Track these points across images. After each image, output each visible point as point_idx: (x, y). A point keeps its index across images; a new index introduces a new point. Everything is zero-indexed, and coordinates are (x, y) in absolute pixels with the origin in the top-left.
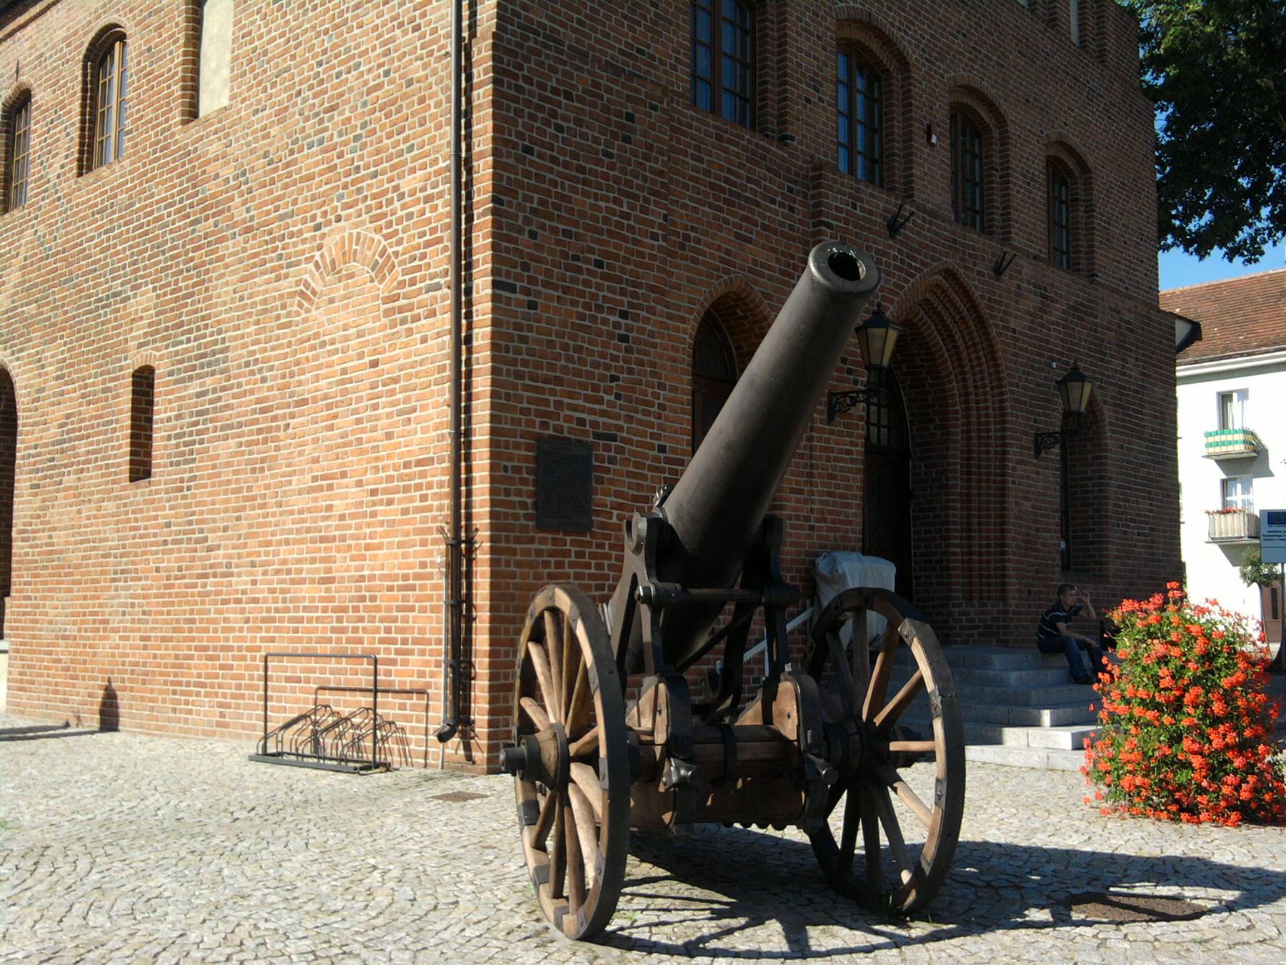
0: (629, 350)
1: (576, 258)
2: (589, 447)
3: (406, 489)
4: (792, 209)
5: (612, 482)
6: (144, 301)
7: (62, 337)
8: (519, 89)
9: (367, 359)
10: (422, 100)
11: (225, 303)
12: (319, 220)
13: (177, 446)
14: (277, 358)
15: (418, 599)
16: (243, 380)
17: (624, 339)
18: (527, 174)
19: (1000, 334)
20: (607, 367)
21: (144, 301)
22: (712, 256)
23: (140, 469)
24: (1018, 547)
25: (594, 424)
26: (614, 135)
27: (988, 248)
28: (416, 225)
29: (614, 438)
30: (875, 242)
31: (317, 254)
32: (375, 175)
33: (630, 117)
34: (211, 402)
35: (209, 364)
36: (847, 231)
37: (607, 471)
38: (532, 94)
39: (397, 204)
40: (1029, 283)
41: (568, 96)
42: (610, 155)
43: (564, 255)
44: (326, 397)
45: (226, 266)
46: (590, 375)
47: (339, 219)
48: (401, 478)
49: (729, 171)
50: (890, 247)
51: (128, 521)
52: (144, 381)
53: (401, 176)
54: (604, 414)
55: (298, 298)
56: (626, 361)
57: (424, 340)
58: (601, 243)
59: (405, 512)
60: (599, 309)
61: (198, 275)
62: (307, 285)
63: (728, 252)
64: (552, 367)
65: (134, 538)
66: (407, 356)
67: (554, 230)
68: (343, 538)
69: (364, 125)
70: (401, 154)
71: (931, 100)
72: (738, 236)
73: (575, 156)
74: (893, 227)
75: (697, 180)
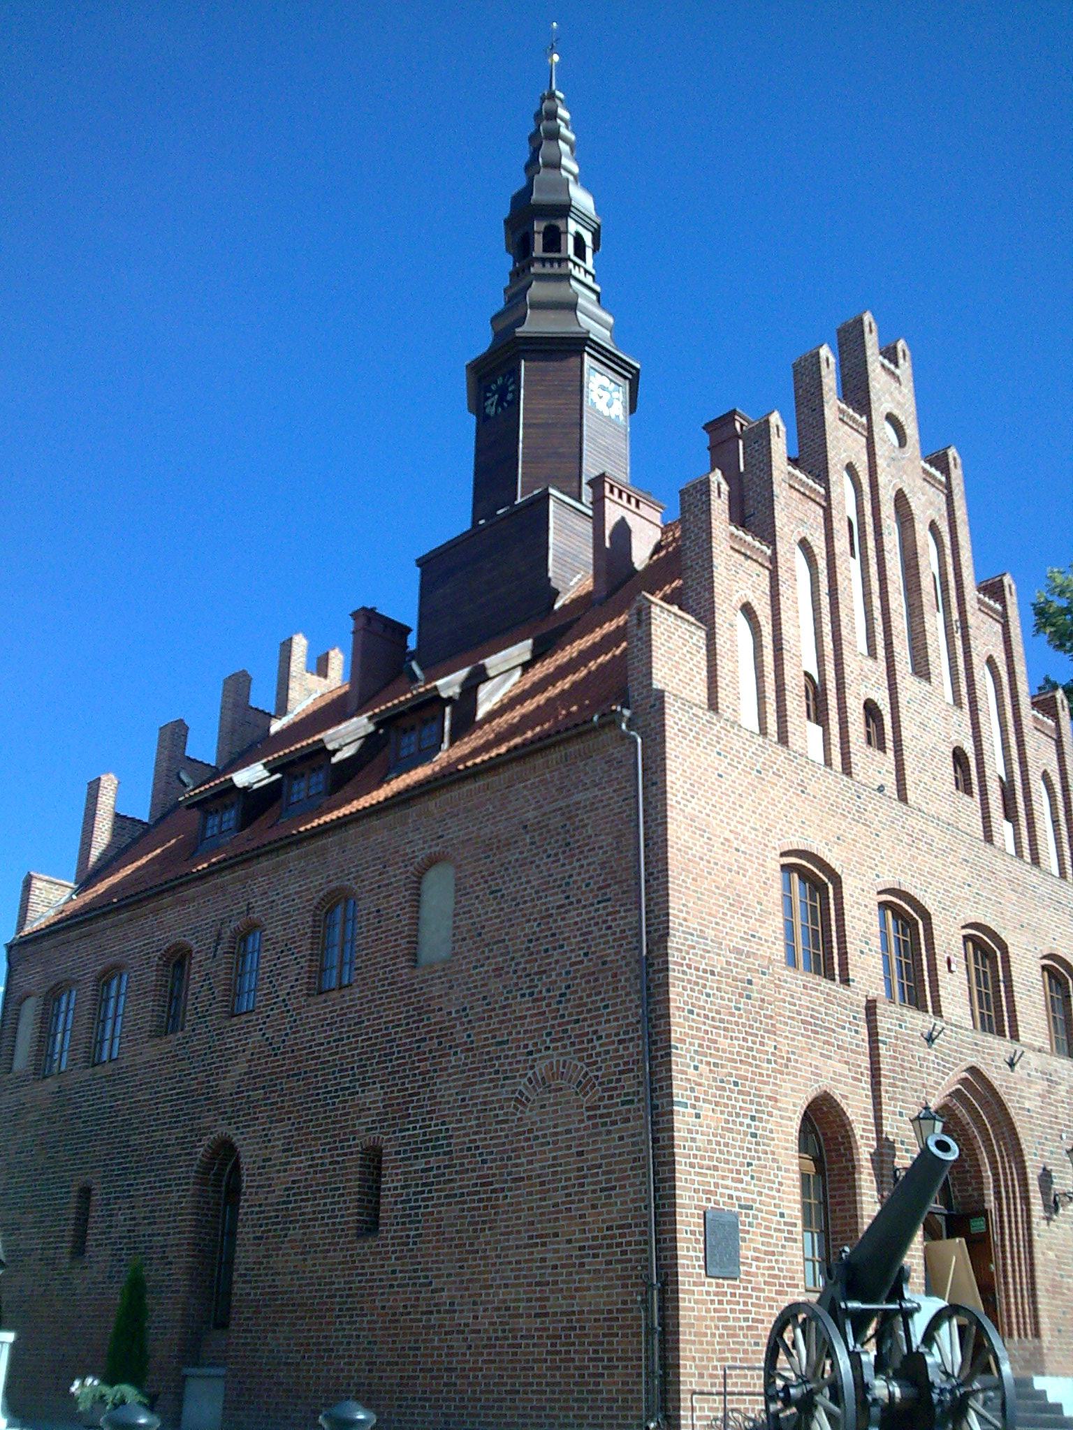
0: (757, 1144)
1: (722, 1081)
2: (736, 1215)
3: (609, 1246)
4: (857, 1032)
5: (751, 1240)
6: (372, 1096)
7: (289, 1119)
8: (684, 973)
9: (574, 1150)
10: (615, 975)
11: (449, 1102)
12: (530, 1048)
13: (404, 1209)
14: (495, 1145)
15: (621, 1327)
16: (466, 1161)
17: (754, 1135)
18: (691, 1028)
19: (1018, 1114)
20: (745, 1157)
21: (372, 1096)
22: (806, 1071)
23: (370, 1225)
24: (1047, 1290)
25: (738, 1199)
26: (741, 995)
27: (1001, 1047)
28: (612, 1059)
29: (751, 1208)
30: (918, 1051)
31: (530, 1073)
32: (577, 1021)
33: (750, 982)
34: (435, 1176)
35: (434, 1147)
36: (896, 1045)
37: (748, 1232)
38: (691, 975)
39: (596, 1043)
40: (1036, 1070)
41: (712, 973)
42: (739, 1009)
43: (715, 1080)
44: (539, 1176)
45: (449, 1075)
46: (734, 1163)
47: (548, 1048)
48: (604, 1238)
49: (813, 1010)
50: (929, 1054)
51: (357, 1268)
52: (373, 1160)
53: (599, 1023)
54: (744, 1190)
55: (513, 1103)
56: (756, 1151)
57: (621, 1138)
58: (736, 1069)
59: (609, 1263)
60: (738, 1115)
61: (424, 1080)
62: (521, 1093)
63: (816, 1067)
64: (711, 1159)
65: (360, 1282)
66: (608, 1149)
67: (708, 1063)
68: (556, 1283)
69: (568, 987)
70: (598, 1009)
71: (948, 941)
72: (822, 1055)
73: (718, 1012)
74: (930, 1039)
75: (793, 1018)
